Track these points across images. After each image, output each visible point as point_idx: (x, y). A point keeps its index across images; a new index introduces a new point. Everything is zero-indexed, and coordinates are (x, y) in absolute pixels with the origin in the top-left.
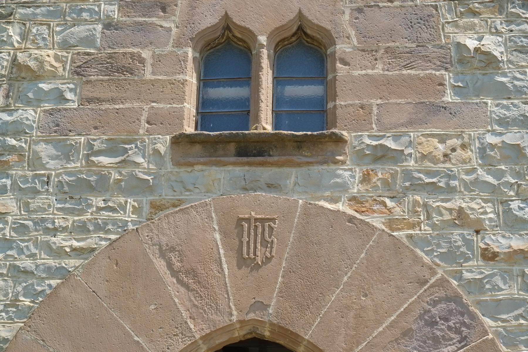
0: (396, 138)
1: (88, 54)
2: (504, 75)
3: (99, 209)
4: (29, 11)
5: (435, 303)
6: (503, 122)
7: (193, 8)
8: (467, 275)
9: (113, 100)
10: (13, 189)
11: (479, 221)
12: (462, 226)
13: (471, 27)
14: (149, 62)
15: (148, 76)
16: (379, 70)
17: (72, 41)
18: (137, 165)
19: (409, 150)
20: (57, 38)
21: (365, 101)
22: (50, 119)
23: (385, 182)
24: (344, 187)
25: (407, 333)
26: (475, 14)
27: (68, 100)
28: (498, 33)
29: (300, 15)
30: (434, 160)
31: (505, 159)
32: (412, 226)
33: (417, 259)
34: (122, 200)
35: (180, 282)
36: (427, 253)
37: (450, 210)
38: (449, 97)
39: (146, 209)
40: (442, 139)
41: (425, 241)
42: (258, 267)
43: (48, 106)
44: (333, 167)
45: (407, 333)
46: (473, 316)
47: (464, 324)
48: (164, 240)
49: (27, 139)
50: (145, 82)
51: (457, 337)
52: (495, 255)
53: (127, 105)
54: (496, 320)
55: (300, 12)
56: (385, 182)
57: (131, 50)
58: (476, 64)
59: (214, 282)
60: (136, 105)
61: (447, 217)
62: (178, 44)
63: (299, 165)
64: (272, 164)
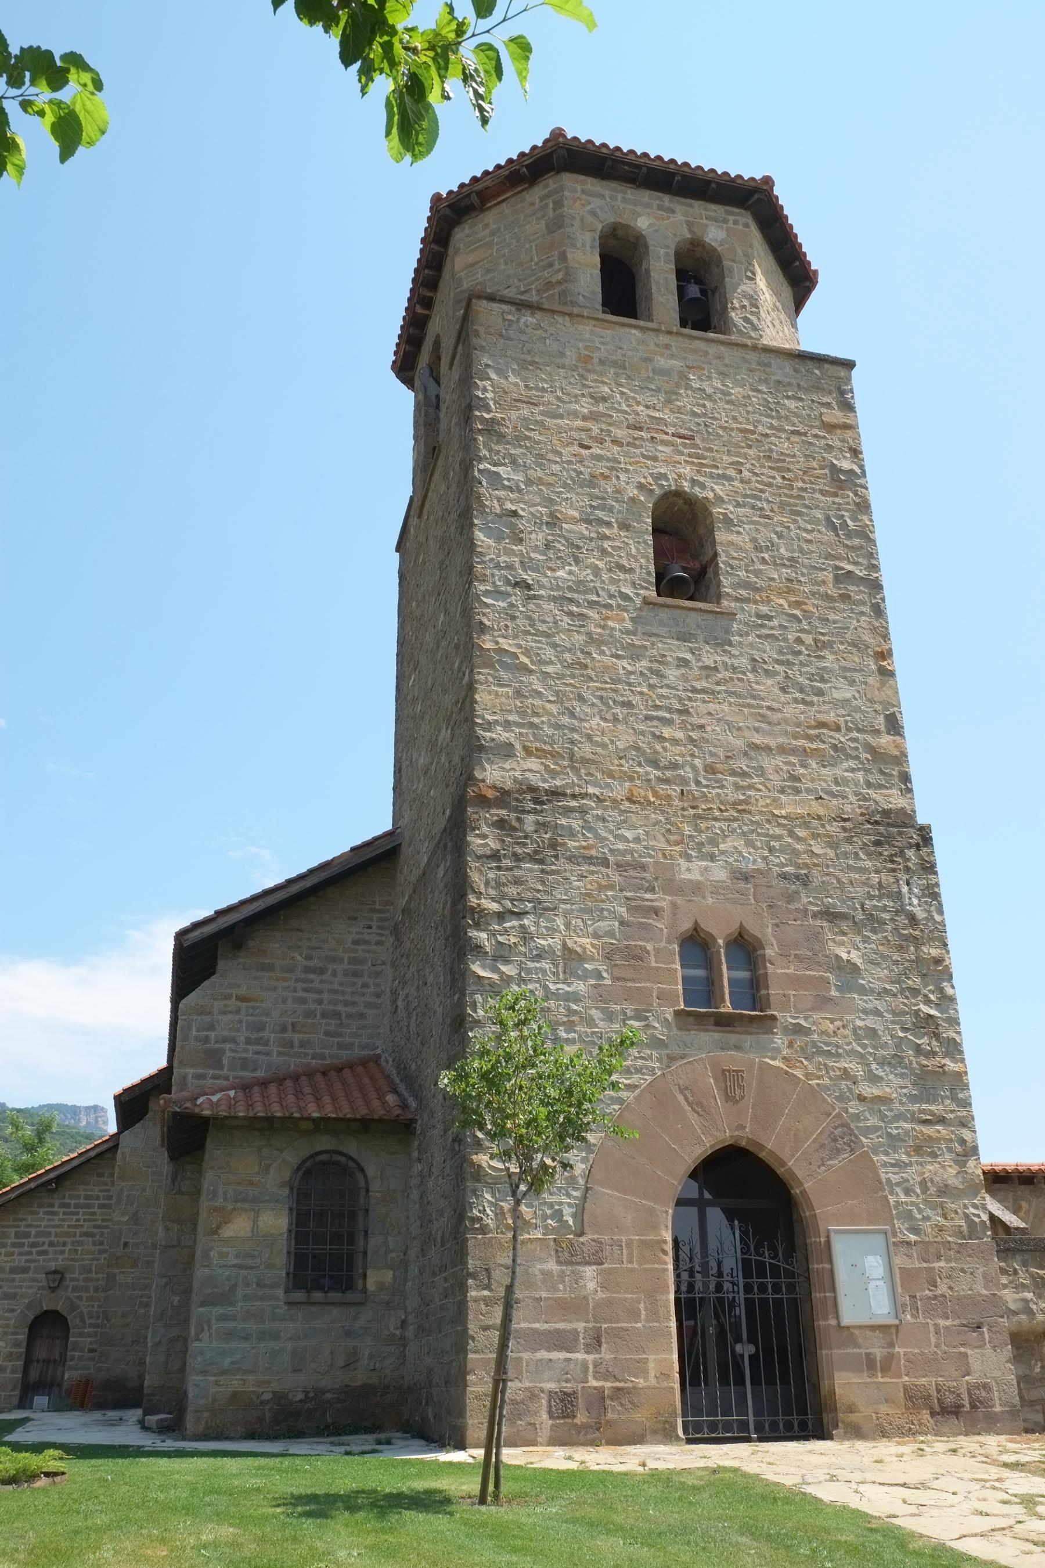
0: (806, 1019)
1: (612, 944)
2: (863, 979)
3: (636, 1058)
4: (568, 906)
5: (836, 1128)
6: (865, 1012)
7: (675, 914)
8: (850, 1110)
9: (633, 980)
10: (580, 1041)
11: (856, 1076)
12: (845, 1079)
13: (842, 944)
14: (652, 953)
15: (654, 964)
16: (791, 971)
17: (600, 933)
18: (655, 1028)
19: (814, 1028)
20: (590, 930)
21: (786, 992)
22: (595, 991)
23: (802, 1048)
24: (778, 1050)
25: (823, 1146)
26: (844, 934)
27: (604, 978)
28: (858, 949)
29: (741, 925)
30: (829, 1036)
31: (867, 1037)
32: (819, 1078)
33: (824, 1100)
34: (649, 1052)
35: (693, 1110)
36: (829, 1095)
37: (839, 1069)
38: (834, 993)
39: (665, 1059)
40: (832, 1021)
41: (827, 1088)
42: (737, 1102)
43: (593, 982)
44: (771, 1036)
45: (823, 1146)
46: (856, 1137)
47: (852, 1141)
48: (681, 1082)
49: (656, 962)
50: (652, 968)
51: (848, 1149)
52: (865, 1098)
53: (643, 985)
54: (867, 1138)
55: (741, 925)
56: (802, 1048)
57: (639, 943)
58: (848, 970)
59: (713, 1110)
60: (648, 985)
61: (838, 1073)
62: (669, 942)
63: (751, 1034)
64: (736, 1033)
